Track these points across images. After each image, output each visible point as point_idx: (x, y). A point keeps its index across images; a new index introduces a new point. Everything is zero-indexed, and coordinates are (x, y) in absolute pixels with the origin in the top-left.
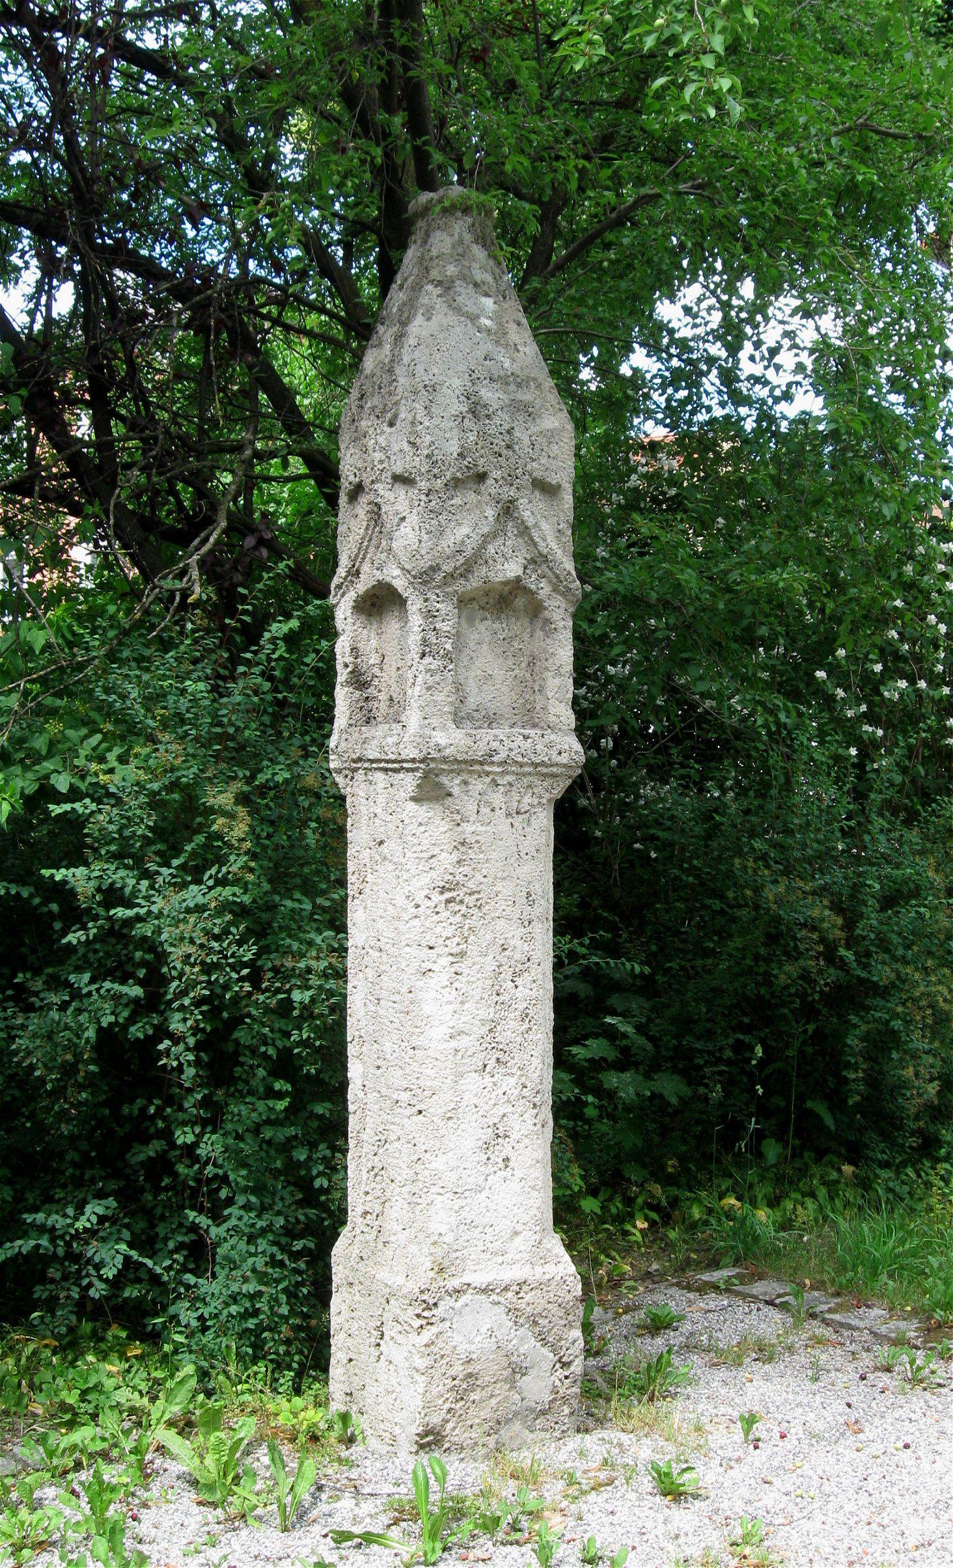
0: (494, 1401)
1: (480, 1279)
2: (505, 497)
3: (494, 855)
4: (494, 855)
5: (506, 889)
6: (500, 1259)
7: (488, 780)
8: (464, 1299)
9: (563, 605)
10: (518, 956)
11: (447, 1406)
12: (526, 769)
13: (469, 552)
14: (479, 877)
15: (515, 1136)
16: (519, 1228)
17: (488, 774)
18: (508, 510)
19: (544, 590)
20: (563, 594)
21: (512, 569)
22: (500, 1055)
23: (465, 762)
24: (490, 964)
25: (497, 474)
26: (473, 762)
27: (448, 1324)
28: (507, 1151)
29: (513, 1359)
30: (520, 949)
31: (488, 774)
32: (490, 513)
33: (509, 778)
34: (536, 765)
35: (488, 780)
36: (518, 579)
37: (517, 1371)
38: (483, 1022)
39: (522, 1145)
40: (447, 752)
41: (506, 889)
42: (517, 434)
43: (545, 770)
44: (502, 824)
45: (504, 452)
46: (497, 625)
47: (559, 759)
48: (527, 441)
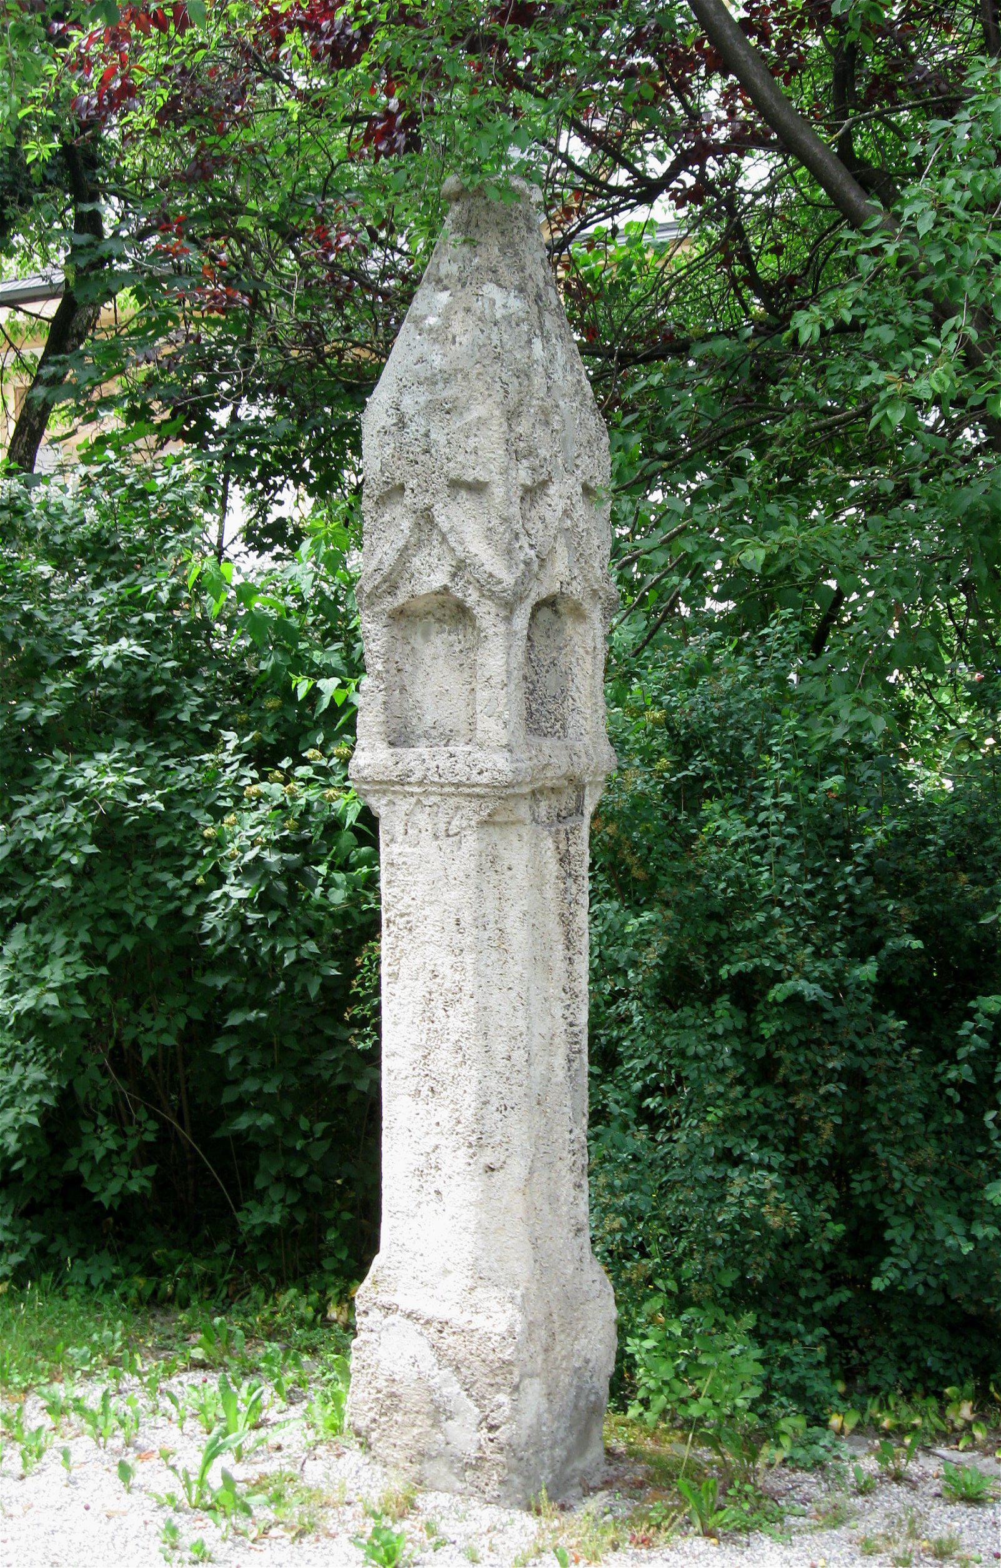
0: (416, 1431)
1: (406, 1305)
2: (421, 506)
3: (421, 878)
4: (421, 878)
5: (433, 913)
6: (431, 1292)
7: (413, 800)
8: (392, 1318)
9: (493, 610)
10: (448, 984)
11: (372, 1414)
12: (447, 790)
13: (386, 569)
14: (407, 899)
15: (445, 1170)
16: (449, 1267)
17: (412, 794)
18: (426, 518)
19: (472, 598)
20: (489, 598)
21: (439, 579)
22: (432, 1083)
23: (381, 782)
24: (421, 991)
25: (412, 483)
26: (392, 783)
27: (374, 1336)
28: (439, 1185)
29: (436, 1397)
30: (450, 978)
31: (412, 794)
32: (406, 524)
33: (434, 799)
34: (458, 785)
35: (413, 800)
36: (446, 588)
37: (439, 1413)
38: (416, 1047)
39: (453, 1182)
40: (365, 773)
41: (433, 913)
42: (433, 436)
43: (467, 791)
44: (429, 847)
45: (422, 458)
46: (453, 638)
47: (476, 779)
48: (443, 440)
